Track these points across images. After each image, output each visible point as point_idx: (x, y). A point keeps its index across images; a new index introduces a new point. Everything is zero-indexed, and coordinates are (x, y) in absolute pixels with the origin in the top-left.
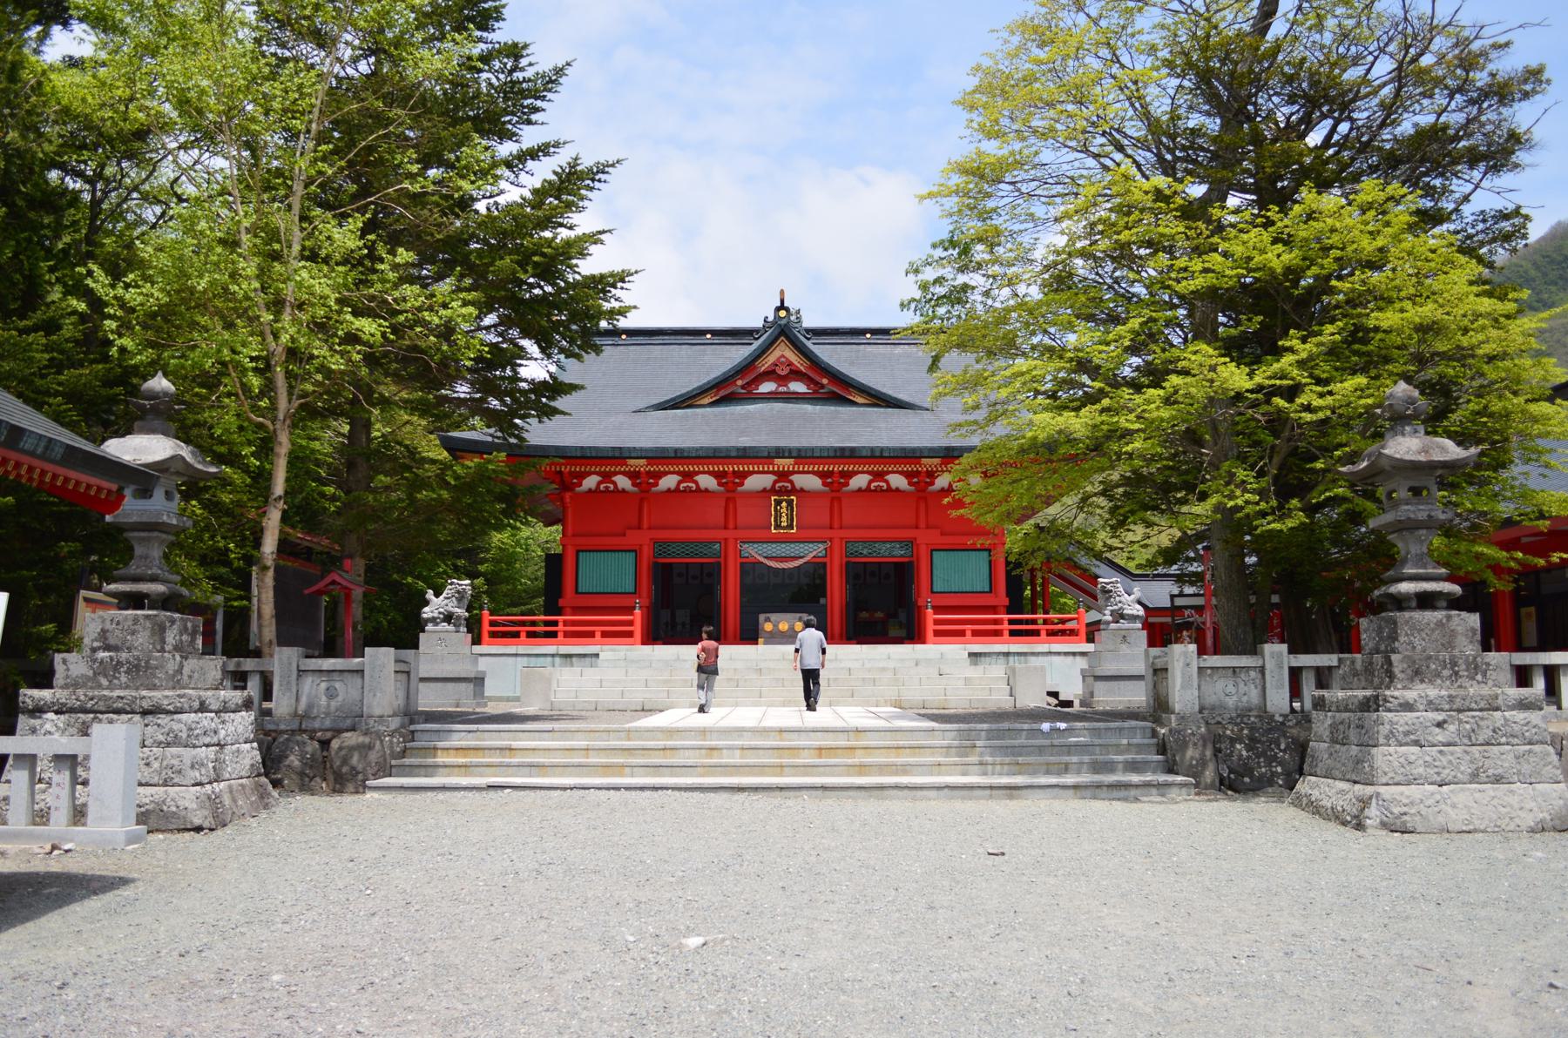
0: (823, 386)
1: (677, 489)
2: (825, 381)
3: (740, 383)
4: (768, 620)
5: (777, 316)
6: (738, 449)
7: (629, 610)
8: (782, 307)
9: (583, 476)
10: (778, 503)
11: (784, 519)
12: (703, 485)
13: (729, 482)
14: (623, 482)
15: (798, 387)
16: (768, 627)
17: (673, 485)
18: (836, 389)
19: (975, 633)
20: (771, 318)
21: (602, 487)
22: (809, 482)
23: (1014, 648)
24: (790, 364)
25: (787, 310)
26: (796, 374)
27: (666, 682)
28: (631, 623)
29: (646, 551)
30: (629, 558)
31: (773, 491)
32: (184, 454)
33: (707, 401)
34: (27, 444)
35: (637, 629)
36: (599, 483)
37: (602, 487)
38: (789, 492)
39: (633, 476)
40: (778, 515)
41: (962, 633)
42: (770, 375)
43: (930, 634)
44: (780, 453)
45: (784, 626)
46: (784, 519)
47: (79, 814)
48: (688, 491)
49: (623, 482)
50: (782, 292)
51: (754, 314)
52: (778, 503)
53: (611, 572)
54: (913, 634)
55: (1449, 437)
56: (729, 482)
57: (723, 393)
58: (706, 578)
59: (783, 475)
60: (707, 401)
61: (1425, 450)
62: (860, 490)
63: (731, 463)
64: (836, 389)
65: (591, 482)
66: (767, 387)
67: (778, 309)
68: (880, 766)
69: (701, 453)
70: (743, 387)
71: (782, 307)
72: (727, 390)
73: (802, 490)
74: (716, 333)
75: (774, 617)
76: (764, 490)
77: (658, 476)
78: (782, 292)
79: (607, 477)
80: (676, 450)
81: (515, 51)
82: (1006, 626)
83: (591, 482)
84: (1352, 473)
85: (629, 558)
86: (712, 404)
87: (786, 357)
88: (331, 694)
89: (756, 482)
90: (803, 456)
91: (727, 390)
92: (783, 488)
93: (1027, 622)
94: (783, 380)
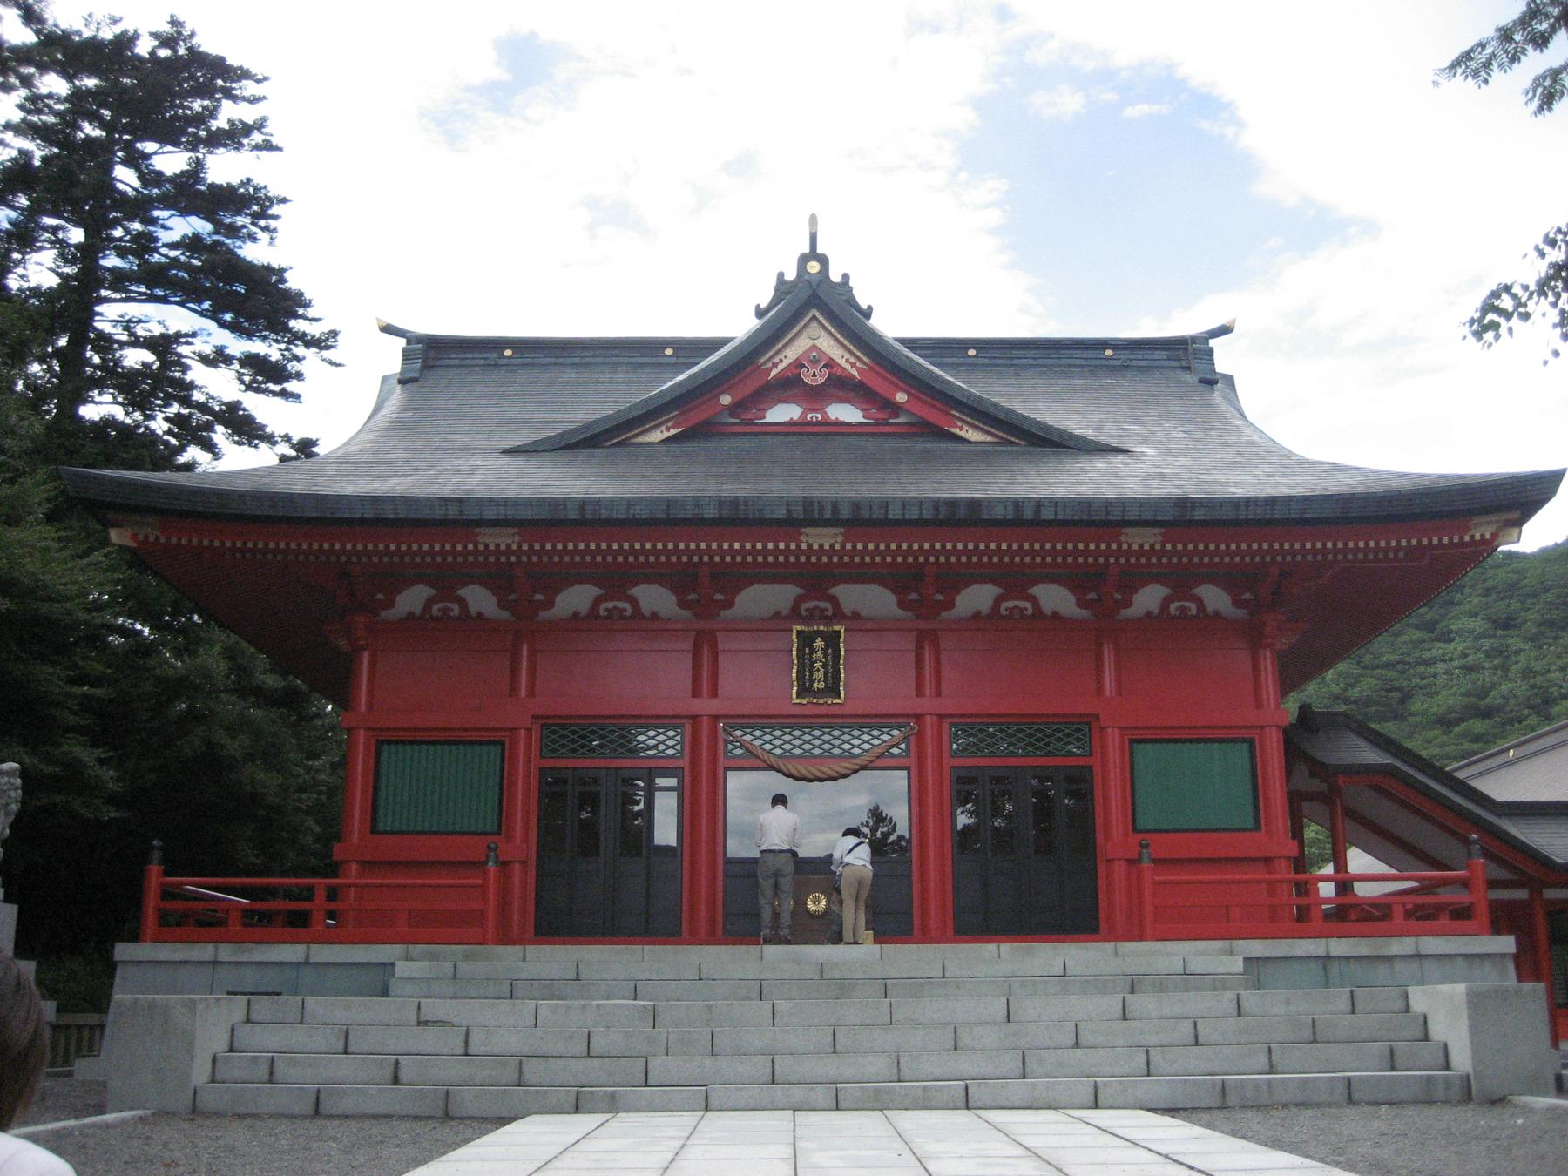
0: (896, 409)
1: (593, 612)
2: (901, 397)
3: (726, 400)
8: (813, 254)
11: (819, 675)
12: (1047, 606)
15: (845, 413)
17: (985, 605)
20: (791, 275)
21: (1173, 607)
23: (1339, 947)
24: (831, 363)
25: (823, 261)
32: (392, 611)
33: (657, 436)
36: (1166, 602)
37: (435, 609)
42: (790, 386)
46: (819, 675)
50: (813, 220)
52: (806, 640)
57: (697, 417)
60: (657, 436)
62: (977, 616)
65: (413, 599)
66: (783, 413)
67: (804, 260)
70: (733, 409)
71: (813, 254)
73: (856, 616)
76: (777, 615)
78: (813, 220)
81: (247, 203)
84: (619, 599)
94: (815, 396)
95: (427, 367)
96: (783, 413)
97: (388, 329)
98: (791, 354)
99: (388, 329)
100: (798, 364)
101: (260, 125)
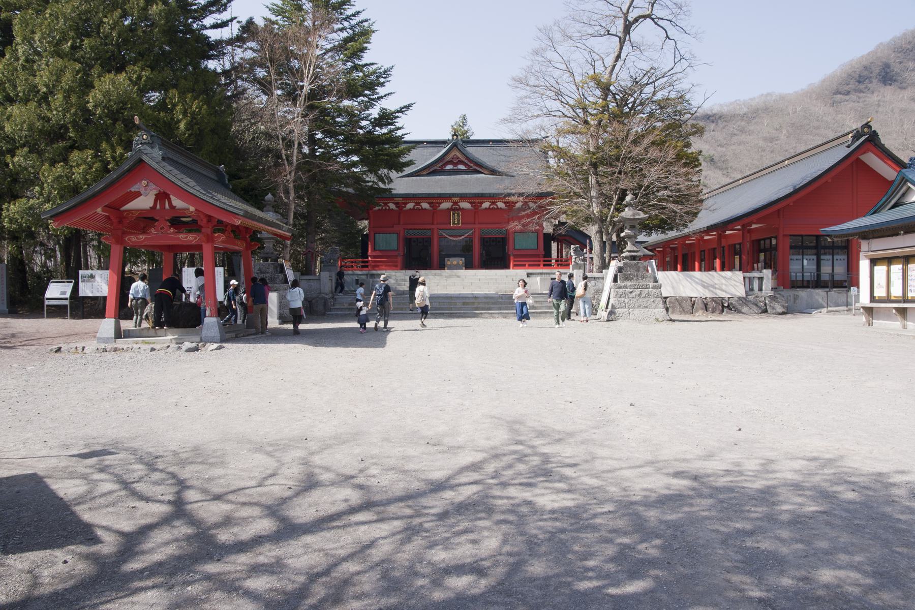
7: (396, 256)
14: (392, 206)
15: (462, 167)
16: (449, 263)
18: (476, 167)
19: (530, 265)
22: (465, 205)
26: (461, 162)
29: (402, 234)
30: (395, 236)
31: (451, 209)
39: (396, 204)
40: (454, 219)
41: (524, 265)
44: (454, 195)
48: (418, 209)
50: (408, 107)
51: (446, 134)
53: (389, 241)
54: (506, 266)
55: (415, 290)
56: (476, 206)
58: (426, 242)
59: (456, 203)
61: (634, 215)
64: (476, 167)
66: (449, 167)
69: (850, 232)
74: (429, 142)
75: (451, 259)
77: (406, 204)
78: (408, 107)
79: (386, 204)
82: (542, 263)
85: (395, 236)
86: (428, 175)
87: (458, 153)
89: (445, 205)
90: (464, 197)
92: (455, 209)
94: (455, 164)
96: (449, 167)
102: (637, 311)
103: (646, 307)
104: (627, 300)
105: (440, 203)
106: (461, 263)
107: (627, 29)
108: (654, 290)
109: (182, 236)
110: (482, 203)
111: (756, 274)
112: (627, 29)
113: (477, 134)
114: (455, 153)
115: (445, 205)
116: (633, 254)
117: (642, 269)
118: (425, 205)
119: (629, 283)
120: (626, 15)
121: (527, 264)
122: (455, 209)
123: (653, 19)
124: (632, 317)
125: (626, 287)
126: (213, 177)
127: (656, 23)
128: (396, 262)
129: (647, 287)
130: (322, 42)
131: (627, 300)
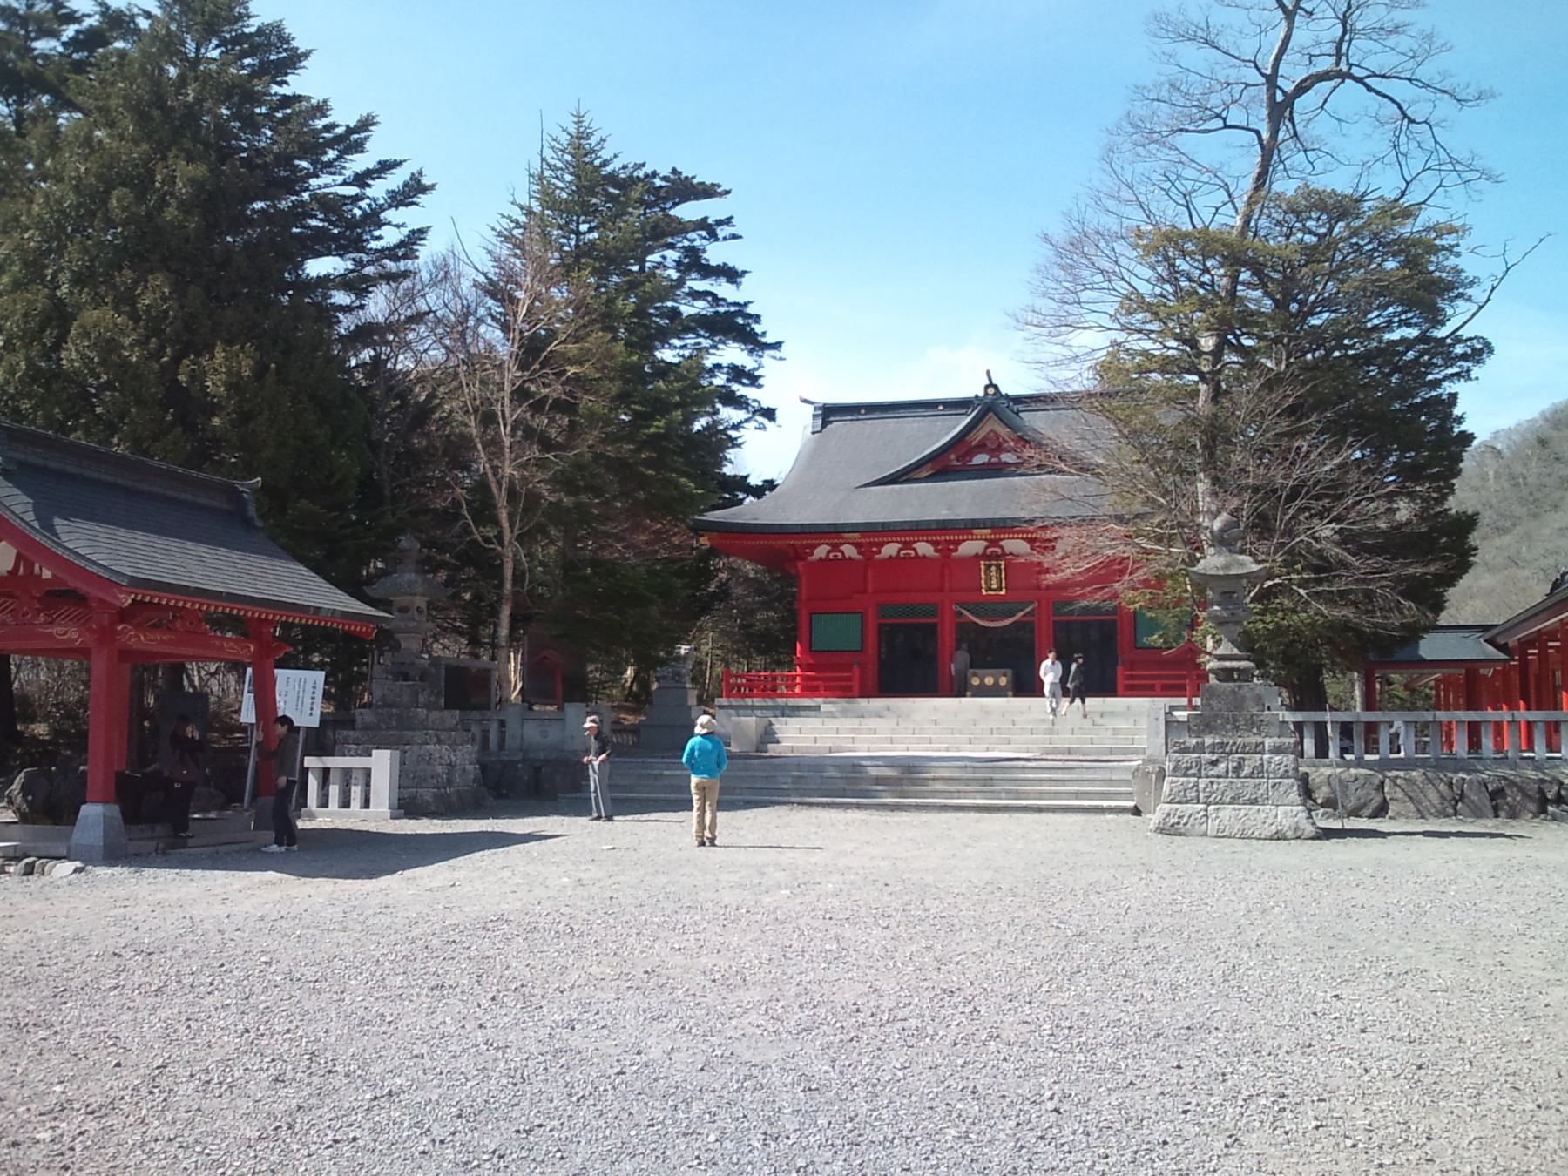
4: (975, 675)
5: (986, 394)
6: (938, 522)
9: (814, 547)
10: (988, 567)
12: (920, 553)
13: (946, 549)
16: (976, 681)
17: (894, 554)
25: (996, 387)
27: (853, 730)
28: (850, 679)
30: (855, 620)
31: (985, 556)
34: (323, 613)
35: (856, 688)
38: (997, 557)
40: (989, 579)
42: (981, 447)
43: (1120, 688)
45: (989, 681)
47: (366, 804)
48: (907, 558)
49: (850, 551)
50: (988, 373)
51: (973, 388)
52: (988, 567)
60: (924, 474)
63: (947, 531)
65: (821, 551)
66: (981, 459)
67: (987, 387)
68: (1007, 792)
71: (991, 385)
72: (942, 465)
78: (988, 373)
79: (835, 547)
80: (883, 524)
83: (821, 551)
85: (855, 620)
86: (928, 479)
88: (544, 734)
89: (970, 547)
91: (942, 465)
92: (993, 555)
93: (843, 679)
95: (825, 424)
96: (981, 459)
97: (805, 401)
98: (987, 429)
99: (805, 401)
100: (985, 438)
101: (728, 221)
102: (1227, 812)
103: (1254, 802)
104: (1202, 783)
105: (958, 543)
106: (1003, 681)
107: (1280, 111)
108: (1277, 758)
109: (56, 630)
110: (881, 545)
111: (1490, 715)
112: (1280, 111)
113: (1009, 388)
114: (992, 425)
115: (970, 547)
116: (1228, 664)
117: (1250, 704)
118: (924, 548)
119: (1208, 741)
120: (1271, 80)
121: (1157, 683)
122: (993, 555)
123: (1360, 80)
124: (1212, 826)
125: (1199, 748)
126: (217, 504)
127: (1370, 89)
128: (850, 679)
129: (1258, 749)
130: (1169, 212)
131: (1202, 783)
